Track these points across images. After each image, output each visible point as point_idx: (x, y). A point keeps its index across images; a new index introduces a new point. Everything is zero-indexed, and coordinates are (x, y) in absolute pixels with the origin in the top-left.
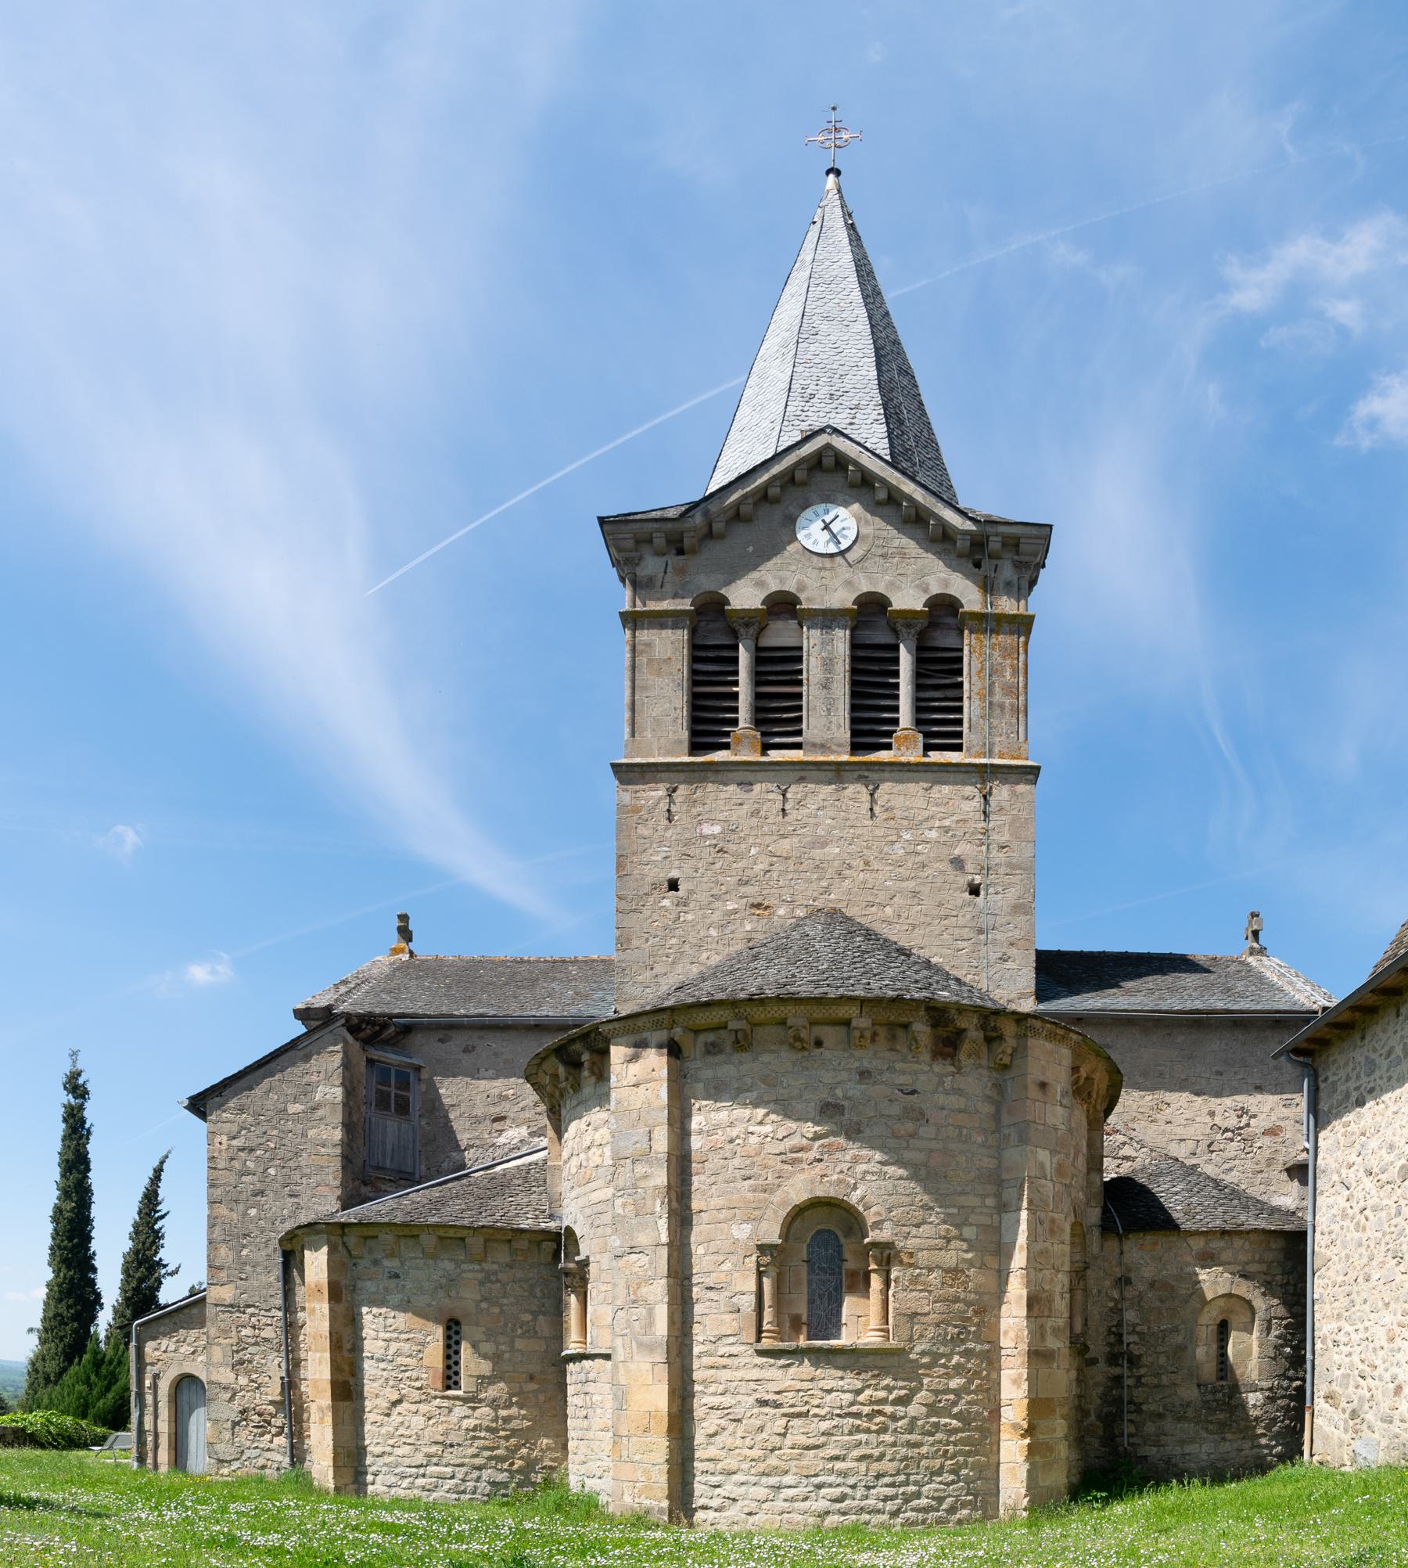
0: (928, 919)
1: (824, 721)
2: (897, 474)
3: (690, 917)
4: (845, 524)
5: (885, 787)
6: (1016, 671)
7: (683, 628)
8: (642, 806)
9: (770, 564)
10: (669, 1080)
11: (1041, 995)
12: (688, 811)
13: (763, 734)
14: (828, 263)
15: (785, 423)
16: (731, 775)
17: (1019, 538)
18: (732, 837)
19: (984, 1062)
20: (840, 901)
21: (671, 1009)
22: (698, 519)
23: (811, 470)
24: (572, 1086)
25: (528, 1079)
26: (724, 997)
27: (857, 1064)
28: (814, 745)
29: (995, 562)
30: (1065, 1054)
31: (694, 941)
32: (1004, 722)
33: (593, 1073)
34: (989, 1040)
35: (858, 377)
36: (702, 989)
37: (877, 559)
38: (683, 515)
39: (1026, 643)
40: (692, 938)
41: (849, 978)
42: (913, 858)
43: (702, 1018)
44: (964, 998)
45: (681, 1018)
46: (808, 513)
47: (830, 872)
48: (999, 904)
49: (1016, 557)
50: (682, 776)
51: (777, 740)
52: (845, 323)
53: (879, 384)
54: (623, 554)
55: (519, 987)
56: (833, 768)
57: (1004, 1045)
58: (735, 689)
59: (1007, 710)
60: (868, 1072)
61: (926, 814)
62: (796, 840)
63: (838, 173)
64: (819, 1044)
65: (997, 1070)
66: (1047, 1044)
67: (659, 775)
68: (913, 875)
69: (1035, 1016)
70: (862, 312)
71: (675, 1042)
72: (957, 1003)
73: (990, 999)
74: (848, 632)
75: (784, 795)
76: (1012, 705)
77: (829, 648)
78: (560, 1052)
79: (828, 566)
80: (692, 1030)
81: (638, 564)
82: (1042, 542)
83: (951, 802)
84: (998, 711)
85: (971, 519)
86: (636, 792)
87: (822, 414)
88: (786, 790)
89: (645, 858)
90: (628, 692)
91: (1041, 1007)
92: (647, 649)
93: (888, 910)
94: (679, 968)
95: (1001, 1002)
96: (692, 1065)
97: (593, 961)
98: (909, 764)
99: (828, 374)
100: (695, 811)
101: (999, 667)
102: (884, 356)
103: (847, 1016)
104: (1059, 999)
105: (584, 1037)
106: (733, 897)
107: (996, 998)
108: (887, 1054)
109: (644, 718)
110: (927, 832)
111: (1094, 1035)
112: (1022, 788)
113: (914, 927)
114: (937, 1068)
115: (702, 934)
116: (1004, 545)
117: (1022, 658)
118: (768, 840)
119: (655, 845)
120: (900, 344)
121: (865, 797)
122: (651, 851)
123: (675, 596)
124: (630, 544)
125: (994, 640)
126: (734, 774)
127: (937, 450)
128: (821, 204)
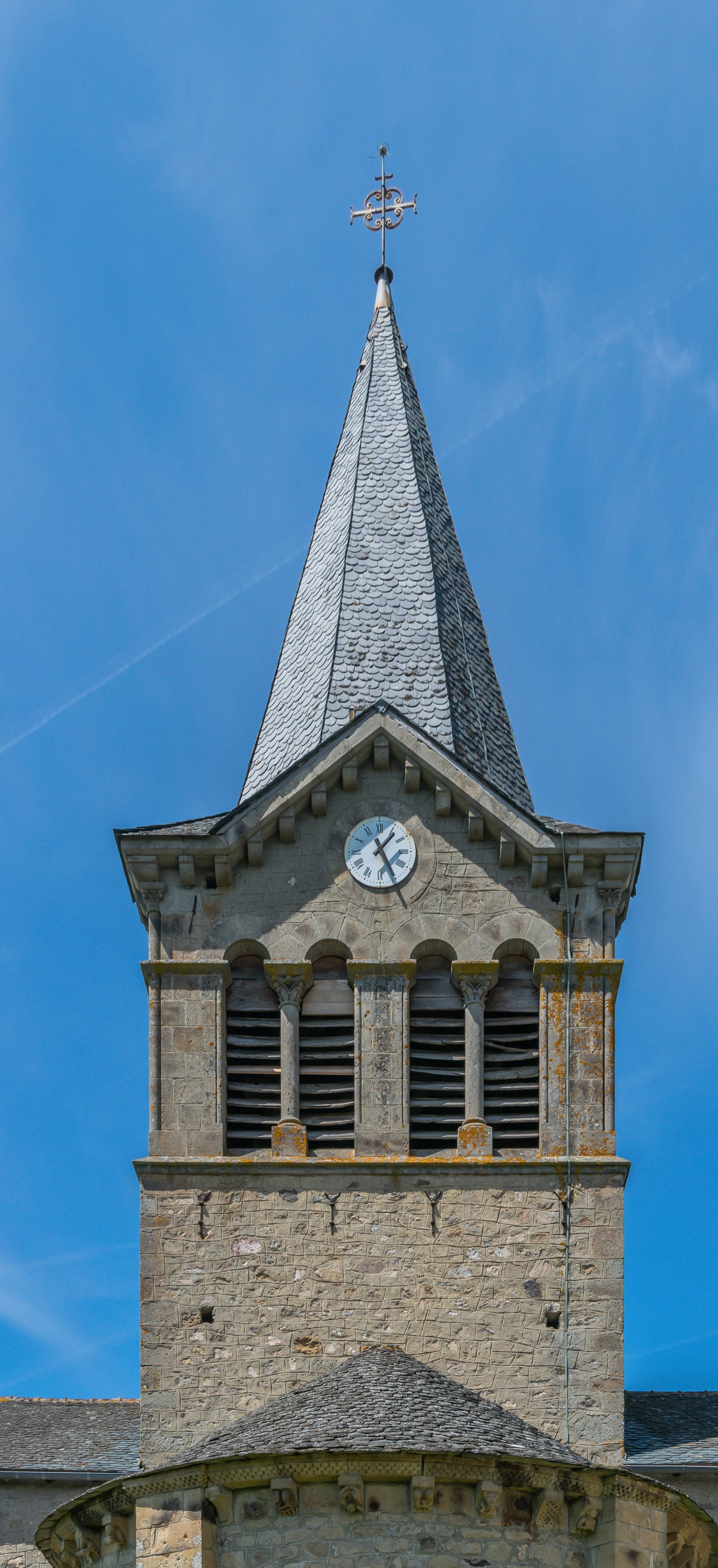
0: (499, 1357)
1: (378, 1112)
2: (462, 772)
3: (226, 1354)
4: (402, 846)
5: (450, 1194)
6: (600, 1040)
7: (216, 988)
8: (171, 1217)
9: (314, 904)
10: (204, 1548)
11: (631, 1447)
12: (223, 1225)
13: (310, 1129)
14: (378, 439)
15: (332, 698)
16: (272, 1180)
17: (604, 856)
18: (274, 1257)
19: (564, 1527)
20: (398, 1335)
21: (206, 1464)
22: (231, 838)
23: (361, 768)
24: (91, 1555)
25: (39, 1545)
26: (266, 1451)
27: (418, 1530)
28: (368, 1143)
29: (575, 891)
30: (659, 1517)
31: (231, 1383)
32: (586, 1109)
33: (115, 1539)
34: (570, 1502)
35: (415, 626)
36: (240, 1441)
37: (439, 894)
38: (214, 831)
39: (613, 1002)
40: (229, 1379)
41: (409, 1429)
42: (481, 1284)
43: (241, 1476)
44: (540, 1452)
45: (216, 1475)
46: (358, 831)
47: (386, 1302)
48: (582, 1337)
49: (600, 883)
50: (216, 1180)
51: (325, 1136)
52: (400, 538)
53: (440, 636)
54: (146, 885)
55: (27, 1434)
56: (389, 1171)
57: (587, 1508)
58: (277, 1070)
59: (591, 1092)
60: (431, 1540)
61: (496, 1228)
62: (347, 1261)
63: (389, 277)
64: (374, 1506)
65: (579, 1537)
66: (638, 1505)
67: (190, 1178)
68: (481, 1303)
69: (624, 1473)
70: (418, 519)
71: (210, 1503)
72: (533, 1457)
73: (572, 1453)
74: (405, 995)
75: (333, 1206)
76: (596, 1085)
77: (384, 1016)
78: (77, 1512)
79: (382, 904)
80: (229, 1489)
81: (162, 899)
82: (631, 858)
83: (525, 1214)
84: (579, 1094)
85: (549, 832)
86: (163, 1199)
87: (374, 684)
88: (335, 1200)
89: (174, 1281)
90: (152, 1071)
91: (632, 1461)
92: (174, 1015)
93: (453, 1346)
94: (214, 1415)
95: (584, 1455)
96: (230, 1531)
97: (115, 1405)
98: (476, 1166)
99: (381, 622)
100: (231, 1225)
101: (580, 1036)
102: (445, 591)
103: (406, 1474)
104: (652, 1450)
105: (105, 1496)
106: (275, 1330)
107: (578, 1451)
108: (452, 1519)
109: (171, 1107)
110: (497, 1251)
111: (694, 1494)
112: (608, 1192)
113: (483, 1366)
114: (510, 1535)
115: (240, 1375)
116: (586, 866)
117: (608, 1021)
118: (315, 1261)
119: (185, 1266)
120: (464, 570)
121: (426, 1208)
122: (180, 1273)
123: (206, 945)
124: (151, 870)
125: (574, 1000)
126: (276, 1179)
127: (509, 734)
128: (371, 334)
